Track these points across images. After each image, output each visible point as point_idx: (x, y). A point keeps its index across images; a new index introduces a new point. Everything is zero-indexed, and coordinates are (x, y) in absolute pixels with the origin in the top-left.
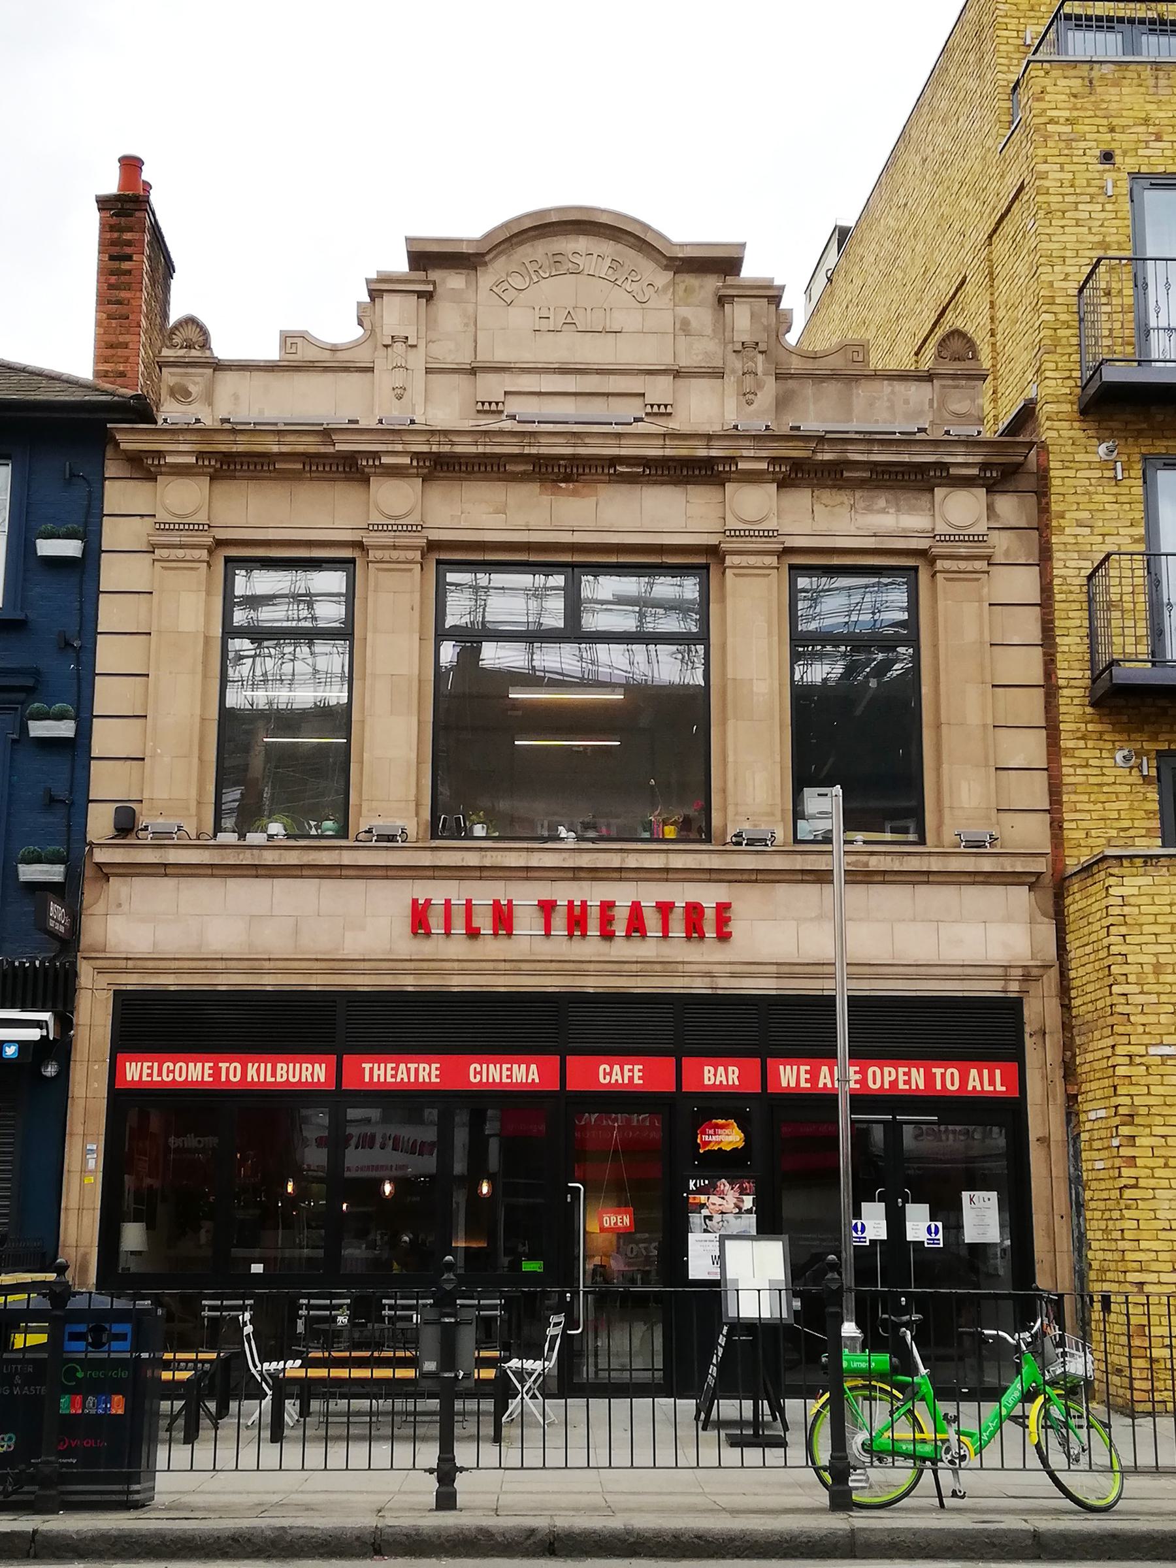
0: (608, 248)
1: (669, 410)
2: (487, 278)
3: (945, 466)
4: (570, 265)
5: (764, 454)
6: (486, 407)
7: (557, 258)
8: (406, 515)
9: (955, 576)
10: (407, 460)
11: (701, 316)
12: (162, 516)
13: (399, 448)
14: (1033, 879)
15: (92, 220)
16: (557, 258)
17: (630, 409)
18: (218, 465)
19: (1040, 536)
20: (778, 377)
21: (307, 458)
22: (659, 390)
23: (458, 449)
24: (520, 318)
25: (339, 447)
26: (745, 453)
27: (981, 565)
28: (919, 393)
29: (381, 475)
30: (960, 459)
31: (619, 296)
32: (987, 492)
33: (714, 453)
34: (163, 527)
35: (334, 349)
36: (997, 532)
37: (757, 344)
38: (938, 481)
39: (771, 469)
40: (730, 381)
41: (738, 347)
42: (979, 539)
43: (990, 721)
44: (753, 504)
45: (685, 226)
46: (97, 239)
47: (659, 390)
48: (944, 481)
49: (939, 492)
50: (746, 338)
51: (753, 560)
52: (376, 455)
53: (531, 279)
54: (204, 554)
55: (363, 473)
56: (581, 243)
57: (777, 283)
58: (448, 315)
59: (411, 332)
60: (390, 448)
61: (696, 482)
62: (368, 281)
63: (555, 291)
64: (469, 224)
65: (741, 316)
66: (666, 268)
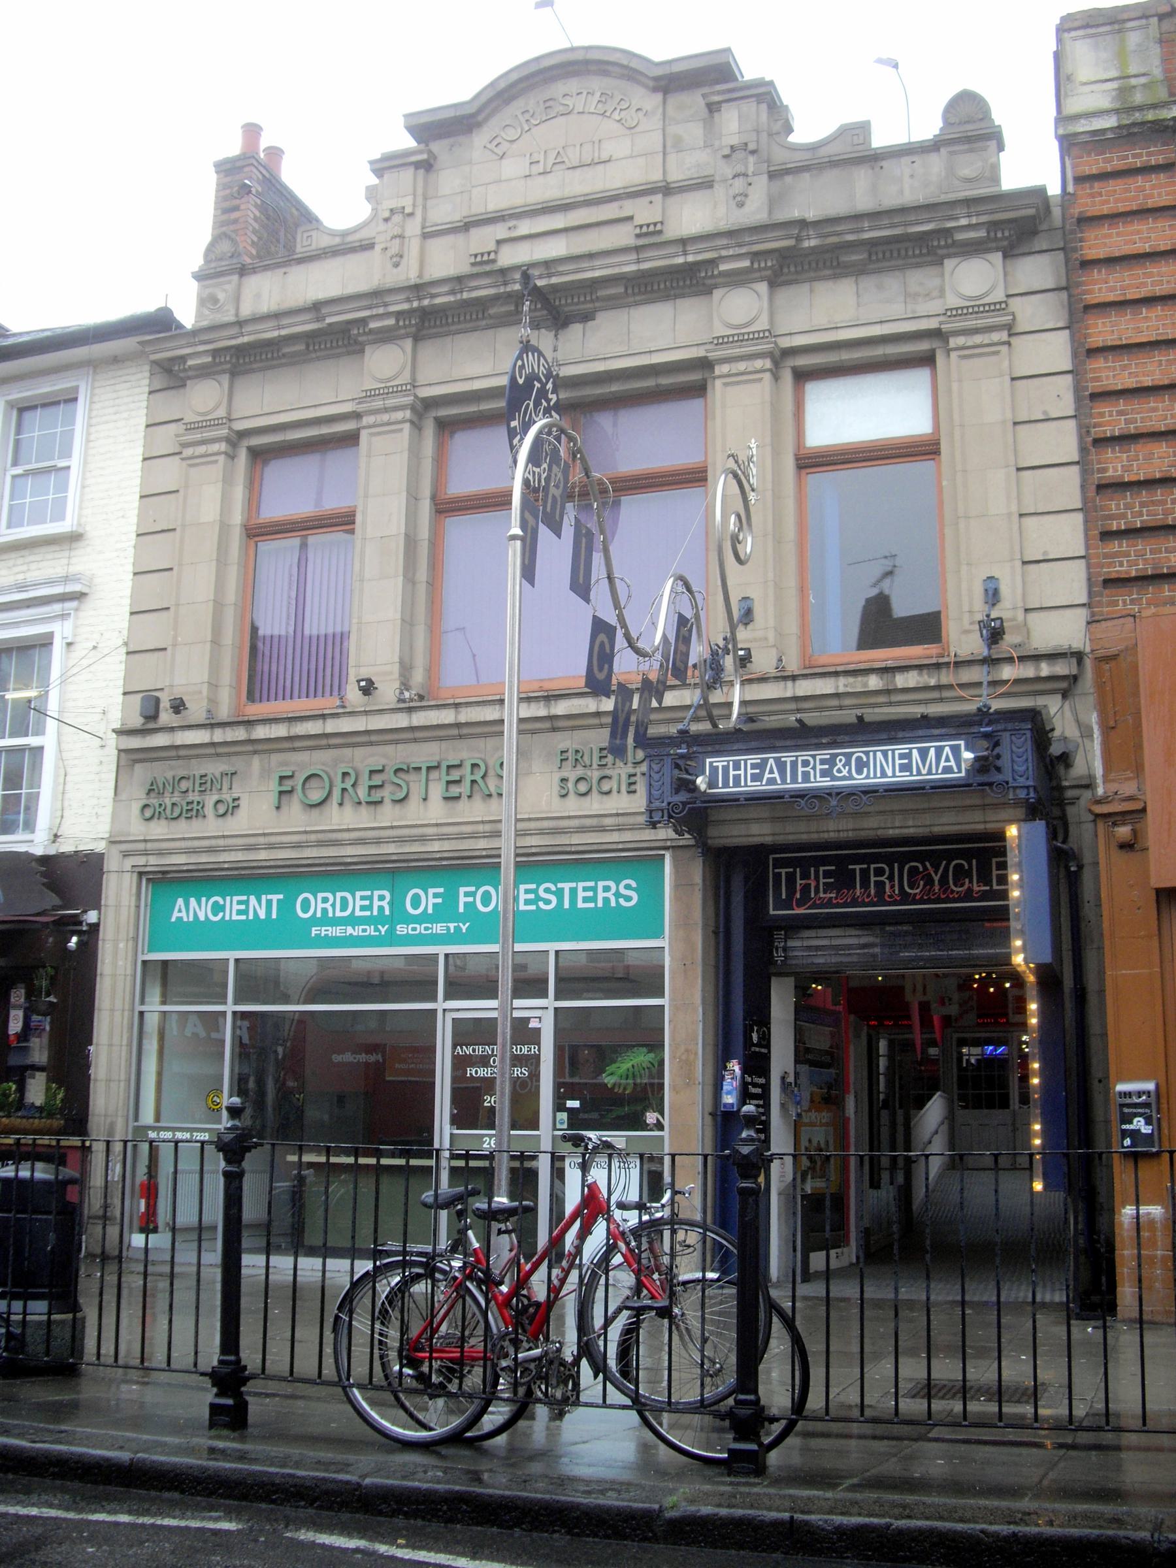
0: (597, 84)
1: (659, 227)
2: (480, 139)
3: (948, 232)
4: (561, 108)
5: (744, 250)
6: (479, 259)
7: (548, 104)
8: (395, 378)
9: (968, 352)
10: (391, 322)
11: (693, 132)
12: (190, 417)
13: (381, 310)
14: (1064, 685)
15: (209, 183)
16: (548, 104)
17: (623, 236)
18: (234, 360)
19: (1070, 296)
20: (773, 175)
21: (310, 338)
22: (645, 212)
23: (438, 301)
24: (513, 167)
25: (329, 320)
26: (724, 253)
27: (1003, 335)
28: (936, 164)
29: (375, 342)
30: (964, 222)
31: (610, 126)
32: (1005, 257)
33: (690, 258)
34: (191, 427)
35: (344, 234)
36: (1018, 299)
37: (746, 144)
38: (944, 251)
39: (756, 266)
40: (719, 191)
41: (727, 151)
42: (999, 308)
43: (1014, 508)
44: (741, 307)
45: (665, 43)
46: (213, 198)
47: (645, 212)
48: (952, 250)
49: (949, 264)
50: (735, 140)
51: (742, 366)
52: (363, 321)
53: (522, 129)
54: (223, 446)
55: (356, 342)
56: (572, 85)
57: (767, 79)
58: (448, 180)
59: (407, 203)
60: (375, 311)
61: (683, 296)
62: (371, 163)
63: (550, 135)
64: (459, 88)
65: (733, 124)
66: (655, 90)
